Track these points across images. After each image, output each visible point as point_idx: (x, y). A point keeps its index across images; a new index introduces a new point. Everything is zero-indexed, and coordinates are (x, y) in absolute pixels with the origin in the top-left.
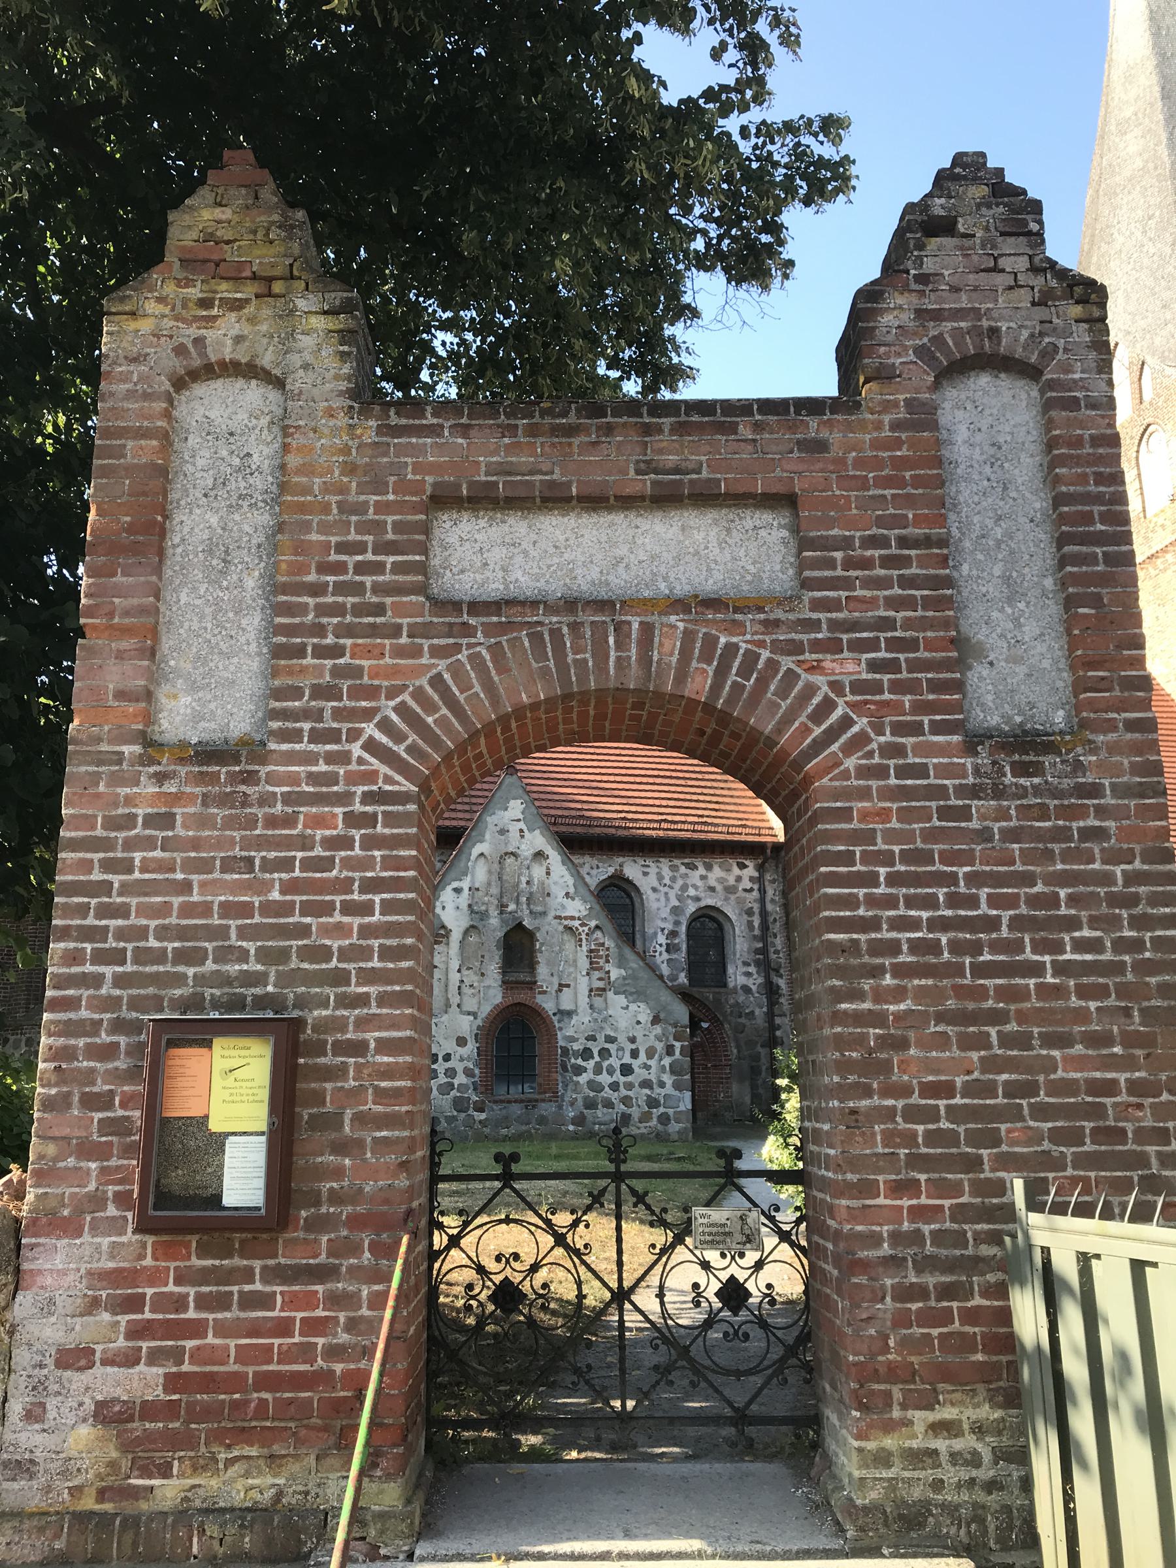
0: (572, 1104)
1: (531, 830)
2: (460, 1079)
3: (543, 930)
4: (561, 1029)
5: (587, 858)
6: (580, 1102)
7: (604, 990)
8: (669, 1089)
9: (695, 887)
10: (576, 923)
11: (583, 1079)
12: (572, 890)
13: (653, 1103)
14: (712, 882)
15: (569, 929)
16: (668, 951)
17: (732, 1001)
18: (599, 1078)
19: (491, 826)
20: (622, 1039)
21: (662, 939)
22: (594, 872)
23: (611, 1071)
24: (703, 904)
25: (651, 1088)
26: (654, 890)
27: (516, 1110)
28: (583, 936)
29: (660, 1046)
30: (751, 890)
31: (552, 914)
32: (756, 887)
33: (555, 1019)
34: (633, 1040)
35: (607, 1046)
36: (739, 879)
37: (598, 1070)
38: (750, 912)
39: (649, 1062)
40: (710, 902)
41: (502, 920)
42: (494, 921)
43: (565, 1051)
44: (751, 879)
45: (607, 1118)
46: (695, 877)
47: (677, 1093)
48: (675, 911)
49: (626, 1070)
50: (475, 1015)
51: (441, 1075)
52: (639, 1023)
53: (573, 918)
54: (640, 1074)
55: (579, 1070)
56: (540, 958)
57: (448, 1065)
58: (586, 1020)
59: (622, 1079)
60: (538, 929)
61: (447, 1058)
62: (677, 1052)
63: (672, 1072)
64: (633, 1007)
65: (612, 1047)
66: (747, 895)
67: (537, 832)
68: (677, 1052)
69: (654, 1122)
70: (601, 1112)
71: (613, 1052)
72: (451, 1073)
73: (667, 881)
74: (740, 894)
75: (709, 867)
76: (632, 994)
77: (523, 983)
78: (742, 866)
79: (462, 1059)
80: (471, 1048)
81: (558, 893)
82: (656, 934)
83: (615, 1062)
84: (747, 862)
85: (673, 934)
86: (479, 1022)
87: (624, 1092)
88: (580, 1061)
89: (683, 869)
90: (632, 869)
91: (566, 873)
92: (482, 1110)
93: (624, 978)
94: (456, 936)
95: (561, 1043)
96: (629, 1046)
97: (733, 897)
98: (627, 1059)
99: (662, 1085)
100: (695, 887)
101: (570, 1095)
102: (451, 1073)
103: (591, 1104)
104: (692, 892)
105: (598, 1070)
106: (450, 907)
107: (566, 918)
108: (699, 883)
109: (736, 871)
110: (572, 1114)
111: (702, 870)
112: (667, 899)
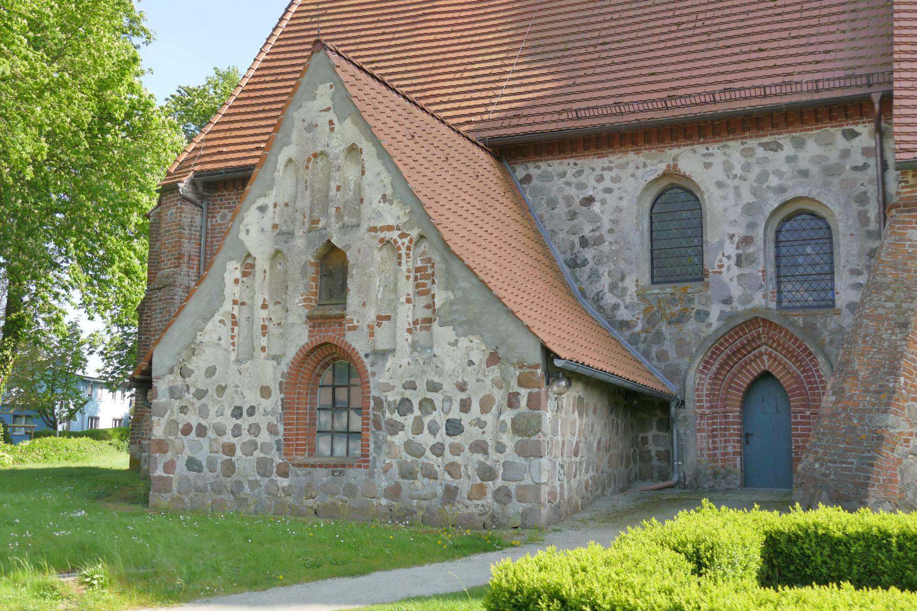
0: (385, 471)
1: (341, 119)
2: (265, 437)
3: (354, 249)
4: (374, 374)
5: (631, 156)
6: (395, 469)
7: (430, 320)
8: (510, 454)
9: (779, 173)
10: (395, 234)
11: (399, 439)
12: (389, 192)
13: (487, 473)
14: (804, 162)
15: (385, 242)
16: (739, 263)
17: (832, 326)
18: (419, 439)
19: (298, 124)
20: (448, 387)
21: (730, 249)
22: (640, 172)
23: (433, 431)
24: (789, 195)
25: (486, 453)
26: (720, 185)
27: (322, 476)
28: (403, 251)
29: (499, 396)
30: (865, 166)
31: (365, 225)
32: (872, 161)
33: (367, 362)
34: (462, 387)
35: (430, 395)
36: (845, 154)
37: (418, 428)
38: (862, 199)
39: (484, 418)
40: (800, 192)
41: (309, 241)
42: (300, 242)
43: (379, 403)
44: (866, 152)
45: (426, 492)
46: (778, 160)
47: (521, 461)
48: (749, 209)
49: (454, 428)
50: (277, 358)
51: (245, 432)
52: (471, 363)
53: (390, 228)
54: (472, 433)
55: (395, 428)
56: (351, 284)
57: (252, 420)
58: (405, 361)
59: (448, 440)
60: (349, 246)
61: (252, 411)
62: (523, 402)
63: (516, 431)
64: (464, 342)
65: (437, 398)
66: (858, 175)
67: (348, 121)
68: (523, 402)
69: (489, 499)
70: (421, 483)
71: (438, 404)
72: (255, 429)
73: (738, 171)
74: (848, 174)
75: (799, 144)
76: (461, 324)
77: (329, 317)
78: (851, 135)
79: (266, 413)
80: (277, 397)
81: (373, 196)
82: (721, 244)
83: (439, 417)
84: (858, 129)
85: (747, 241)
86: (284, 368)
87: (449, 457)
88: (396, 416)
89: (760, 152)
90: (690, 160)
91: (382, 168)
92: (285, 475)
93: (452, 303)
94: (262, 264)
95: (374, 393)
96: (460, 396)
97: (836, 181)
98: (455, 413)
99: (500, 448)
100: (779, 173)
101: (384, 459)
102: (255, 429)
103: (408, 473)
104: (774, 181)
105: (418, 428)
106: (254, 230)
107: (382, 229)
108: (785, 168)
109: (842, 143)
110: (384, 485)
111: (788, 149)
112: (738, 195)
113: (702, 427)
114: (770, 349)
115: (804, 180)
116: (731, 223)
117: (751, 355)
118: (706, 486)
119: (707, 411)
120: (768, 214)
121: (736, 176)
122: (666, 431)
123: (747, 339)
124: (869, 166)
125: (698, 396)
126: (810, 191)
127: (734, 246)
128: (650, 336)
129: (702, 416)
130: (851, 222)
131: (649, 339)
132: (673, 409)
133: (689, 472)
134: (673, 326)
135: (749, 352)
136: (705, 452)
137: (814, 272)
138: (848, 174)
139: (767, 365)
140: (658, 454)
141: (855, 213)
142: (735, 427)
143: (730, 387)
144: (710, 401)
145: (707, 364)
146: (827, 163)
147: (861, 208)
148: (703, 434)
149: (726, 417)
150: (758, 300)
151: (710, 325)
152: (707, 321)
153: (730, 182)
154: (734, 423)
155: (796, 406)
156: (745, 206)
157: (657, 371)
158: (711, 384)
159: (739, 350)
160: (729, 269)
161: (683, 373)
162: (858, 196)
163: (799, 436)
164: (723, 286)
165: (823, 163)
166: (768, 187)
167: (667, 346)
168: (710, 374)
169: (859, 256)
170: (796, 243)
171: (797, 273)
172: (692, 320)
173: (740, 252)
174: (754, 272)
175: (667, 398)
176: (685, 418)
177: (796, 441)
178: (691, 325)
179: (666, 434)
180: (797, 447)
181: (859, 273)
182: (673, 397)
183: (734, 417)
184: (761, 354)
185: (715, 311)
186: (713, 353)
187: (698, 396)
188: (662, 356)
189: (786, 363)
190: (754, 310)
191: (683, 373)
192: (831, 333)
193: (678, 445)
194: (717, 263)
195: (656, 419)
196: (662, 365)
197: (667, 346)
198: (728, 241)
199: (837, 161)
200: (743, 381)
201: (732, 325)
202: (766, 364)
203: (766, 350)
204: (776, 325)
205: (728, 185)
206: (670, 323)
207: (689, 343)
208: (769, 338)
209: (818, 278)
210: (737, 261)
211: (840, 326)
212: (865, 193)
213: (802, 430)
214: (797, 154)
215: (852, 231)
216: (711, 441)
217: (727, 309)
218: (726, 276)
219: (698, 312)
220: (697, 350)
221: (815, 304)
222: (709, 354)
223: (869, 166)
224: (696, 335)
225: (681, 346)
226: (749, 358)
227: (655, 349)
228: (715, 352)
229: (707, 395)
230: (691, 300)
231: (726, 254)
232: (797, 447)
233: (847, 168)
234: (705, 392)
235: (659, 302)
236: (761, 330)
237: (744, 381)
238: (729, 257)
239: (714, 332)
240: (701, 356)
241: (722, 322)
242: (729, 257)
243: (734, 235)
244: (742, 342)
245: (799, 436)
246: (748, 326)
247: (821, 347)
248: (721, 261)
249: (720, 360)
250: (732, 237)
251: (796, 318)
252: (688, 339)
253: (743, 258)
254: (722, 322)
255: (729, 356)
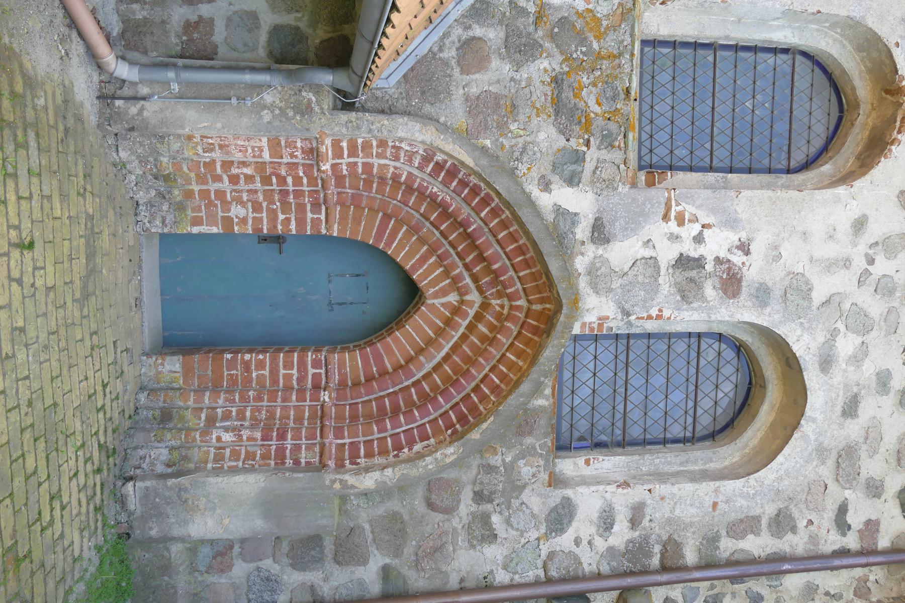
9: (857, 359)
16: (683, 262)
17: (526, 470)
21: (718, 244)
24: (812, 377)
26: (860, 225)
30: (842, 526)
32: (852, 541)
36: (875, 489)
44: (871, 527)
48: (798, 290)
66: (830, 515)
73: (883, 266)
82: (732, 223)
85: (731, 283)
97: (826, 472)
104: (846, 345)
112: (831, 266)
113: (286, 152)
114: (471, 313)
115: (838, 410)
116: (776, 248)
117: (459, 269)
118: (123, 154)
119: (326, 167)
120: (781, 331)
121: (871, 261)
122: (270, 54)
123: (503, 270)
124: (844, 535)
125: (367, 145)
126: (814, 420)
127: (723, 254)
128: (526, 24)
129: (313, 153)
130: (741, 502)
131: (520, 22)
132: (326, 78)
133: (151, 110)
134: (548, 90)
135: (467, 267)
136: (217, 155)
137: (630, 406)
138: (836, 494)
139: (436, 302)
140: (204, 24)
141: (757, 511)
142: (293, 226)
143: (387, 217)
144: (353, 173)
145: (450, 171)
146: (864, 455)
147: (764, 522)
148: (266, 156)
149: (316, 207)
150: (596, 309)
151: (546, 186)
152: (555, 178)
153: (862, 248)
154: (301, 222)
155: (342, 364)
156: (807, 282)
157: (435, 37)
158: (395, 178)
159: (473, 246)
160: (674, 238)
161: (427, 109)
162: (791, 518)
163: (274, 371)
164: (634, 223)
165: (864, 447)
166: (834, 333)
167: (500, 69)
168: (422, 178)
169: (669, 521)
170: (693, 371)
171: (631, 372)
172: (562, 142)
173: (709, 267)
174: (660, 298)
175: (357, 61)
176: (305, 110)
177: (261, 365)
178: (547, 136)
179: (262, 52)
180: (247, 365)
181: (634, 523)
182: (363, 79)
183: (316, 222)
184: (462, 292)
185: (579, 201)
186: (475, 191)
187: (367, 145)
188: (472, 54)
189: (440, 348)
190: (576, 301)
191: (427, 109)
192: (510, 468)
193: (231, 85)
194: (689, 209)
195: (303, 25)
196: (450, 53)
197: (500, 69)
198: (734, 238)
199: (864, 475)
200: (401, 247)
201: (546, 247)
202: (438, 300)
203: (471, 304)
204: (538, 349)
205: (855, 245)
206: (557, 81)
207: (502, 127)
208: (499, 316)
209: (618, 416)
210: (689, 259)
211: (524, 487)
212: (794, 529)
213: (288, 377)
214: (891, 395)
215: (721, 506)
216: (248, 171)
217: (582, 231)
218: (657, 230)
219: (579, 158)
220: (484, 150)
221: (566, 409)
222: (473, 180)
223: (844, 535)
224: (524, 150)
225: (495, 109)
226: (454, 266)
227: (493, 35)
228: (478, 193)
229: (367, 167)
230: (608, 142)
231: (706, 232)
232: (247, 365)
233: (848, 493)
234: (376, 162)
235: (611, 57)
236: (522, 302)
237: (403, 252)
238: (699, 239)
239: (528, 196)
240: (470, 162)
241: (550, 217)
242: (699, 239)
243: (747, 253)
244: (496, 257)
245: (274, 371)
246: (534, 277)
247: (484, 448)
248: (694, 219)
249: (455, 203)
250: (744, 248)
251: (548, 391)
252: (513, 127)
253: (693, 274)
254: (550, 217)
255: (464, 224)
